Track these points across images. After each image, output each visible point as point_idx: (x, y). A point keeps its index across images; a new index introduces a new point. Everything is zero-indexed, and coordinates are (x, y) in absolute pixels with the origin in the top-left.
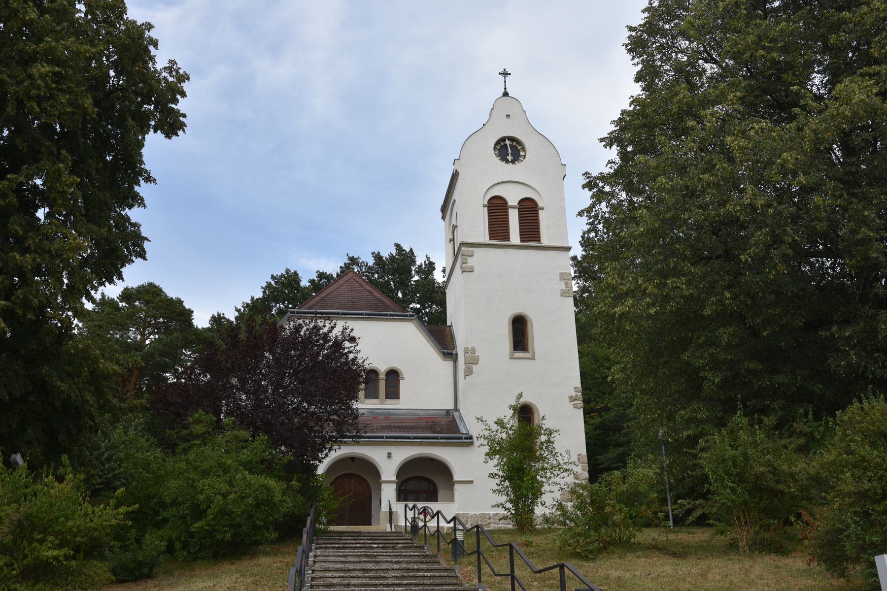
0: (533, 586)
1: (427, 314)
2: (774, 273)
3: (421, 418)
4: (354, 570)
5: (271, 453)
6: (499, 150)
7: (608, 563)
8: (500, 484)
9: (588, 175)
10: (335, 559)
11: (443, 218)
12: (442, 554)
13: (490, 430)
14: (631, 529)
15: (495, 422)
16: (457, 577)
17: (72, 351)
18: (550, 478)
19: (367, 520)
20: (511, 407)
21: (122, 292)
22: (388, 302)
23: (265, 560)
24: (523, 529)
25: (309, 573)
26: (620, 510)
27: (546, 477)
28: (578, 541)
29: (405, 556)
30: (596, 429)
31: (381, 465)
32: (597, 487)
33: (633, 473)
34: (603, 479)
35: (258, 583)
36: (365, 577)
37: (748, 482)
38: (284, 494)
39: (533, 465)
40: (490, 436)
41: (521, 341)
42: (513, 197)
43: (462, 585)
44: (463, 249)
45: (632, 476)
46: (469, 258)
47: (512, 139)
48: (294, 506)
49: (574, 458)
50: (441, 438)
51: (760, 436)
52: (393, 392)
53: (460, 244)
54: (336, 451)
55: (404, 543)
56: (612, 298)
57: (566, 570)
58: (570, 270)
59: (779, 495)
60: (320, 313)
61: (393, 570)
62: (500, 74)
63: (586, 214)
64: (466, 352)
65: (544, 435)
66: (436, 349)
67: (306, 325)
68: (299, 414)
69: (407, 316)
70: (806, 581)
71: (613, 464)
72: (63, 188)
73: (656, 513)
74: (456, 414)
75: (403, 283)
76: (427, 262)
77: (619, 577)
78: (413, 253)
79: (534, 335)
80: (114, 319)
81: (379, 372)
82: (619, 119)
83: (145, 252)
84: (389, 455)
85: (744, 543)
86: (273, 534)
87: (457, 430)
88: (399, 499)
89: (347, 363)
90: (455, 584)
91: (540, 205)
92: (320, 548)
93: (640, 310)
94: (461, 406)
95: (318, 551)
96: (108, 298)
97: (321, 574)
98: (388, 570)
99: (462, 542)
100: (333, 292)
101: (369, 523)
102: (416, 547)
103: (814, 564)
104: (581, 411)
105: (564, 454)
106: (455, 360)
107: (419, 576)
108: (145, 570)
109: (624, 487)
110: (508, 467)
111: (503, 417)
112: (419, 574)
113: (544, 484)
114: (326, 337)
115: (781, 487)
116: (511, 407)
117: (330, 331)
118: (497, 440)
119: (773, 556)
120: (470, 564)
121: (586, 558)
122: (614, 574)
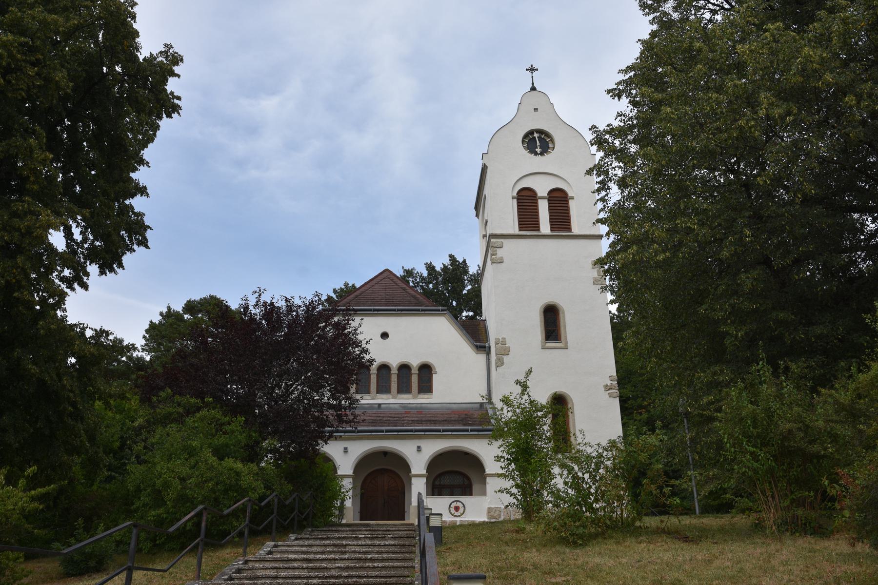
2: (800, 196)
3: (453, 412)
6: (528, 143)
11: (477, 215)
17: (42, 332)
19: (401, 514)
21: (185, 305)
24: (530, 517)
29: (379, 545)
31: (410, 459)
37: (773, 445)
41: (554, 331)
42: (542, 188)
44: (492, 240)
47: (540, 131)
50: (472, 431)
51: (788, 388)
52: (426, 387)
59: (815, 461)
64: (497, 344)
66: (469, 342)
70: (846, 567)
72: (35, 165)
73: (661, 488)
75: (456, 293)
79: (567, 325)
80: (177, 328)
81: (411, 366)
83: (147, 240)
84: (419, 449)
85: (772, 523)
91: (570, 194)
93: (647, 258)
96: (174, 311)
98: (335, 560)
101: (404, 519)
103: (859, 547)
106: (488, 353)
107: (368, 567)
108: (92, 563)
112: (367, 564)
115: (816, 448)
119: (809, 538)
121: (575, 544)
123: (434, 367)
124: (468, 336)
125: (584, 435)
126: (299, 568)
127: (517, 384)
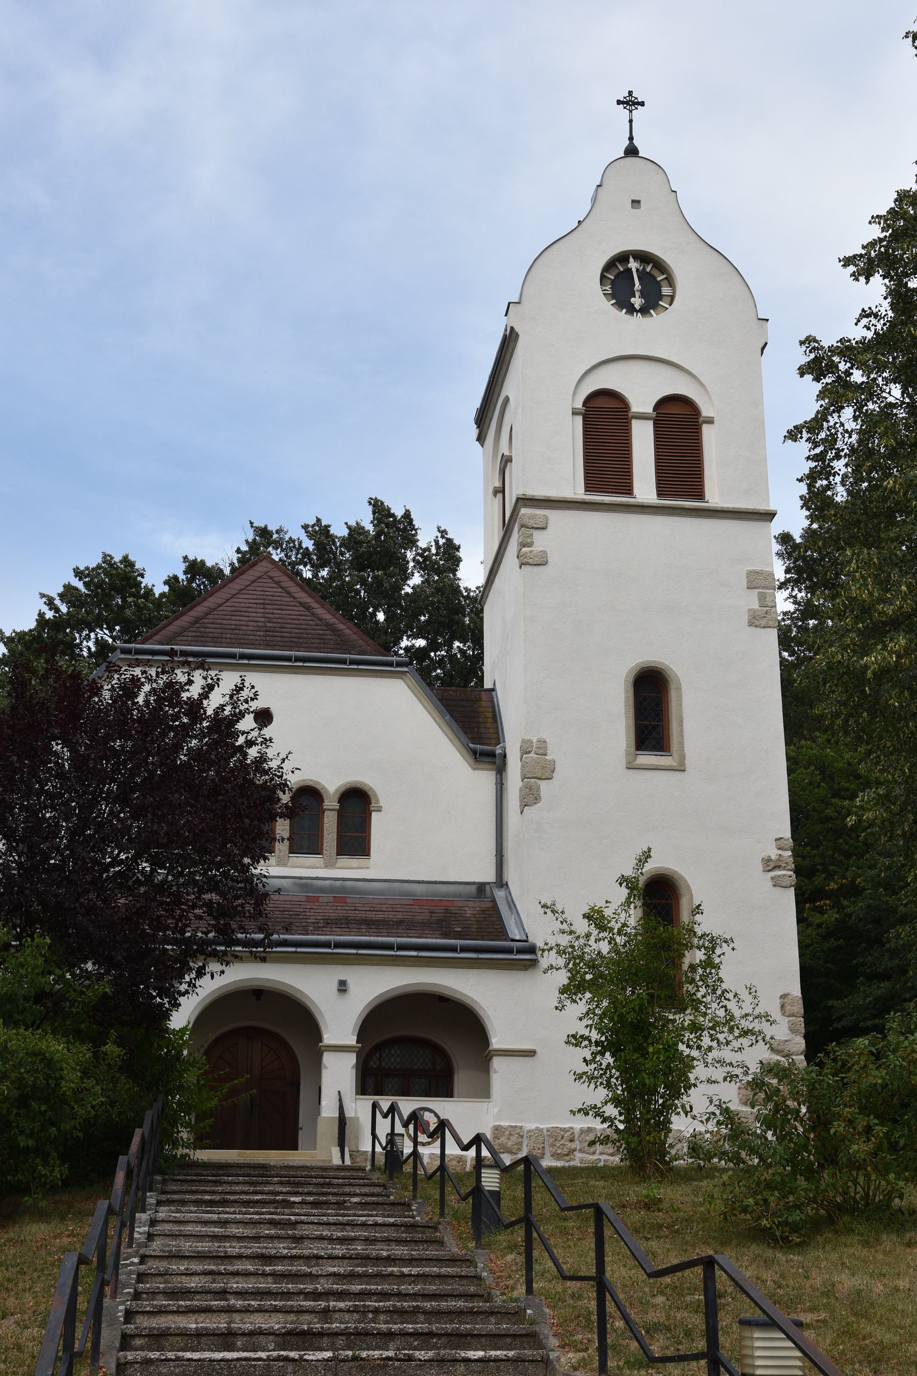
0: (654, 1306)
1: (441, 663)
3: (418, 902)
4: (240, 1257)
5: (61, 979)
6: (613, 283)
7: (835, 1256)
8: (593, 1060)
9: (813, 344)
10: (199, 1228)
11: (481, 439)
12: (449, 1223)
13: (571, 932)
14: (892, 1176)
15: (584, 916)
16: (479, 1278)
18: (710, 1049)
20: (622, 880)
22: (348, 631)
23: (37, 1231)
24: (643, 1167)
25: (132, 1264)
26: (868, 1129)
27: (699, 1048)
28: (766, 1201)
29: (364, 1225)
30: (825, 938)
32: (814, 1075)
33: (898, 1044)
34: (827, 1054)
35: (10, 1286)
36: (264, 1274)
38: (85, 1074)
39: (671, 1017)
40: (572, 947)
41: (654, 728)
43: (488, 1298)
44: (523, 511)
45: (894, 1051)
46: (536, 534)
47: (644, 257)
48: (112, 1103)
49: (770, 1004)
50: (464, 949)
53: (518, 499)
54: (212, 977)
55: (366, 1195)
56: (860, 633)
57: (718, 1273)
58: (771, 564)
60: (184, 653)
61: (331, 1258)
62: (619, 102)
63: (805, 435)
64: (525, 752)
65: (699, 948)
67: (150, 680)
68: (129, 889)
69: (390, 664)
71: (865, 1019)
74: (500, 894)
76: (442, 541)
77: (859, 1292)
78: (411, 520)
79: (685, 715)
81: (322, 791)
82: (891, 211)
84: (343, 987)
86: (57, 1169)
87: (501, 932)
88: (363, 1089)
89: (243, 766)
90: (473, 1296)
91: (706, 412)
92: (168, 1202)
94: (511, 876)
95: (162, 1209)
97: (162, 1265)
98: (318, 1257)
99: (496, 1195)
100: (220, 605)
102: (392, 1204)
104: (791, 894)
105: (744, 995)
107: (391, 1275)
109: (876, 1076)
110: (611, 1020)
111: (604, 905)
112: (390, 1269)
113: (695, 1063)
114: (195, 708)
116: (622, 880)
117: (205, 695)
118: (587, 957)
120: (512, 1248)
121: (784, 1243)
122: (847, 1282)
123: (376, 795)
124: (455, 726)
125: (755, 997)
126: (258, 1274)
127: (621, 884)
